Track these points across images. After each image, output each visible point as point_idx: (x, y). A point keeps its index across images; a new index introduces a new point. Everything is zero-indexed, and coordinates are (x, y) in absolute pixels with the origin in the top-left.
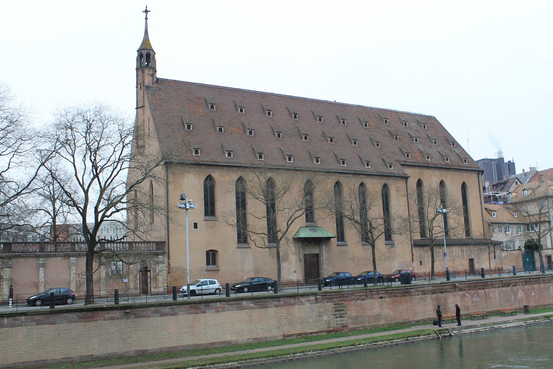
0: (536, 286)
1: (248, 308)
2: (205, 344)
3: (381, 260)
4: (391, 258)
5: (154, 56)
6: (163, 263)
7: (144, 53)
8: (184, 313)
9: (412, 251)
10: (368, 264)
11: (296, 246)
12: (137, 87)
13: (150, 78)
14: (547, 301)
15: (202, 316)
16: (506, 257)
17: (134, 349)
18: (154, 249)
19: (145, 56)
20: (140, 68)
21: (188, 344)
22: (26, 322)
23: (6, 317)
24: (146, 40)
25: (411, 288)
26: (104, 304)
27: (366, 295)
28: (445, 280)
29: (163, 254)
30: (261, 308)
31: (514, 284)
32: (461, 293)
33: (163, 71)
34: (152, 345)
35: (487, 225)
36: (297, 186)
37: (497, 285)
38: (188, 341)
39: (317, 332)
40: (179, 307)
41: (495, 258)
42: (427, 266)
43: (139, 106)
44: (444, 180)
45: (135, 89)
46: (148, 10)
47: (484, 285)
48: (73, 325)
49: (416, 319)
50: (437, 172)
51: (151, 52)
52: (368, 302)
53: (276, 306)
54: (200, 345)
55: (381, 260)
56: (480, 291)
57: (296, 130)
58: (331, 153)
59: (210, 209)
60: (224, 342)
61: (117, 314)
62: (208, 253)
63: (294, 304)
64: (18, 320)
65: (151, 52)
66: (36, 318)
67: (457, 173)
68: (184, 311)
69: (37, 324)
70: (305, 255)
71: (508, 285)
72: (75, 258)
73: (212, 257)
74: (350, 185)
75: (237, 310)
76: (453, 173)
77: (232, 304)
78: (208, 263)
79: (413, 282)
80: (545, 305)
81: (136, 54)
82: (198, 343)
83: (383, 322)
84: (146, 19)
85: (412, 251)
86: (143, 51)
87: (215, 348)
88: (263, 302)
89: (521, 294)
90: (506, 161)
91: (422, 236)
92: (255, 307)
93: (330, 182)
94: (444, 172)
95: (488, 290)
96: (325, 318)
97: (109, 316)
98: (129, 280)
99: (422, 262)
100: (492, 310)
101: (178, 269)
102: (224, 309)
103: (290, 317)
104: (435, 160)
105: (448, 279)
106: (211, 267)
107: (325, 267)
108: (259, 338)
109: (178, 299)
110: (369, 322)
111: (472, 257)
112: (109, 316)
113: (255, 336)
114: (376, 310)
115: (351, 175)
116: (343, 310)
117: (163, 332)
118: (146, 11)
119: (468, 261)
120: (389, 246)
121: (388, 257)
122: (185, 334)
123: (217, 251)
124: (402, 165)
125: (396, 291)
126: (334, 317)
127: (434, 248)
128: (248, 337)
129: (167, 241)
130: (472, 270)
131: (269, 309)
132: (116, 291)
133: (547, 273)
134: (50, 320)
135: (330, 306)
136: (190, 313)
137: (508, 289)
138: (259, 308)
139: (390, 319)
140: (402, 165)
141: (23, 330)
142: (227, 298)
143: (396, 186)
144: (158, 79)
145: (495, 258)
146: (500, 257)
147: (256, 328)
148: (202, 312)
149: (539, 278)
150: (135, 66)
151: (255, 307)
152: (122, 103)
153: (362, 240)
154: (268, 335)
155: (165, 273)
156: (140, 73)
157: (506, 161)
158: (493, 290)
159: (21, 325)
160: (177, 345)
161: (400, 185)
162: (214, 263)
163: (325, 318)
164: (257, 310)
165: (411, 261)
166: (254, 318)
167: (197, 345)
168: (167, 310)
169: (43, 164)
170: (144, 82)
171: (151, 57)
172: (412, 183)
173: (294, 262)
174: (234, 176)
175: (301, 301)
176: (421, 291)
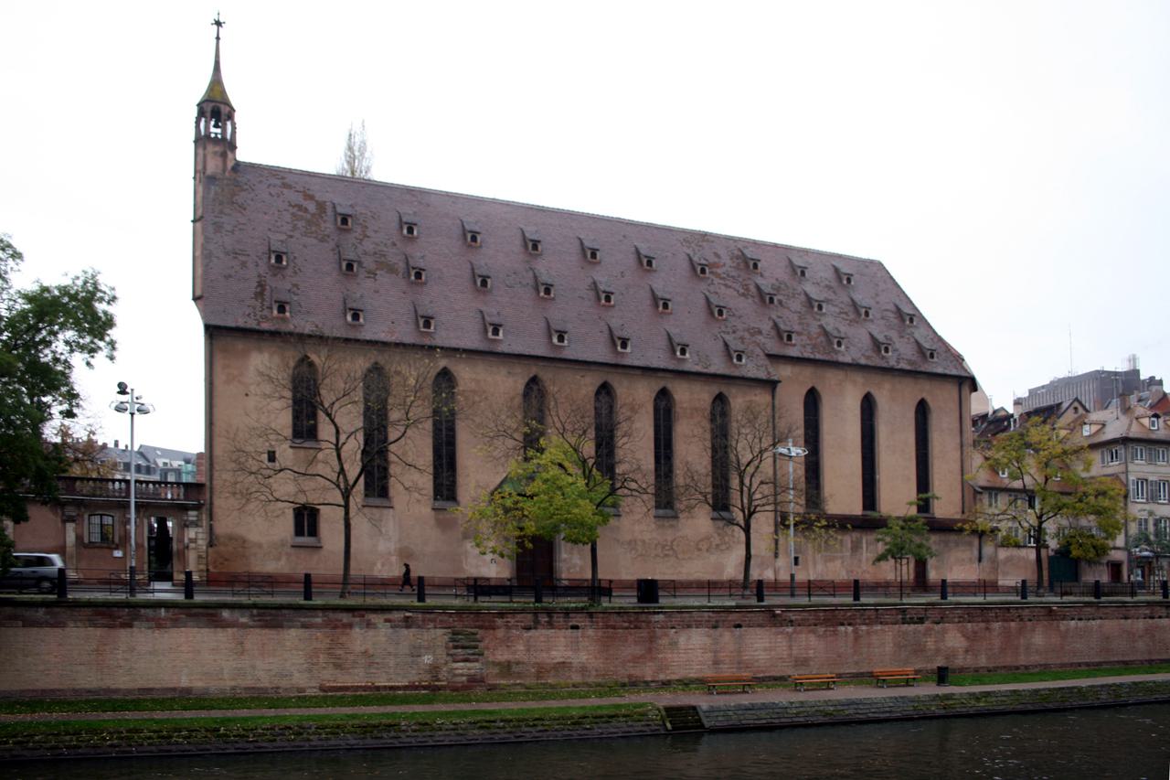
2: (129, 691)
3: (700, 550)
4: (723, 547)
6: (197, 526)
8: (79, 624)
10: (666, 555)
12: (195, 178)
13: (219, 161)
14: (1022, 657)
15: (123, 634)
16: (1008, 560)
18: (182, 497)
23: (165, 607)
24: (216, 81)
28: (850, 600)
29: (198, 507)
35: (972, 492)
36: (504, 385)
38: (88, 679)
39: (405, 688)
41: (980, 560)
45: (193, 181)
47: (942, 615)
50: (859, 378)
52: (540, 634)
54: (117, 691)
55: (700, 550)
57: (531, 274)
58: (603, 323)
60: (174, 689)
63: (350, 626)
65: (222, 107)
68: (80, 621)
74: (637, 397)
75: (207, 627)
78: (299, 531)
79: (949, 598)
80: (1017, 668)
82: (113, 687)
84: (218, 38)
87: (153, 700)
88: (271, 615)
90: (1144, 376)
91: (865, 507)
92: (251, 623)
93: (587, 385)
96: (427, 659)
98: (125, 554)
99: (800, 559)
101: (231, 538)
105: (856, 597)
107: (564, 556)
108: (259, 689)
110: (538, 678)
113: (249, 682)
115: (638, 372)
116: (476, 647)
117: (30, 659)
120: (721, 524)
121: (717, 545)
122: (82, 667)
126: (449, 658)
128: (233, 683)
129: (208, 484)
130: (921, 583)
131: (285, 631)
133: (1031, 599)
135: (439, 636)
136: (95, 626)
137: (920, 627)
140: (770, 356)
142: (187, 601)
144: (238, 164)
145: (980, 560)
146: (994, 560)
147: (253, 667)
149: (1008, 609)
151: (251, 623)
155: (202, 543)
156: (201, 151)
157: (1144, 376)
160: (61, 687)
162: (314, 532)
164: (258, 630)
165: (772, 554)
167: (108, 691)
170: (205, 168)
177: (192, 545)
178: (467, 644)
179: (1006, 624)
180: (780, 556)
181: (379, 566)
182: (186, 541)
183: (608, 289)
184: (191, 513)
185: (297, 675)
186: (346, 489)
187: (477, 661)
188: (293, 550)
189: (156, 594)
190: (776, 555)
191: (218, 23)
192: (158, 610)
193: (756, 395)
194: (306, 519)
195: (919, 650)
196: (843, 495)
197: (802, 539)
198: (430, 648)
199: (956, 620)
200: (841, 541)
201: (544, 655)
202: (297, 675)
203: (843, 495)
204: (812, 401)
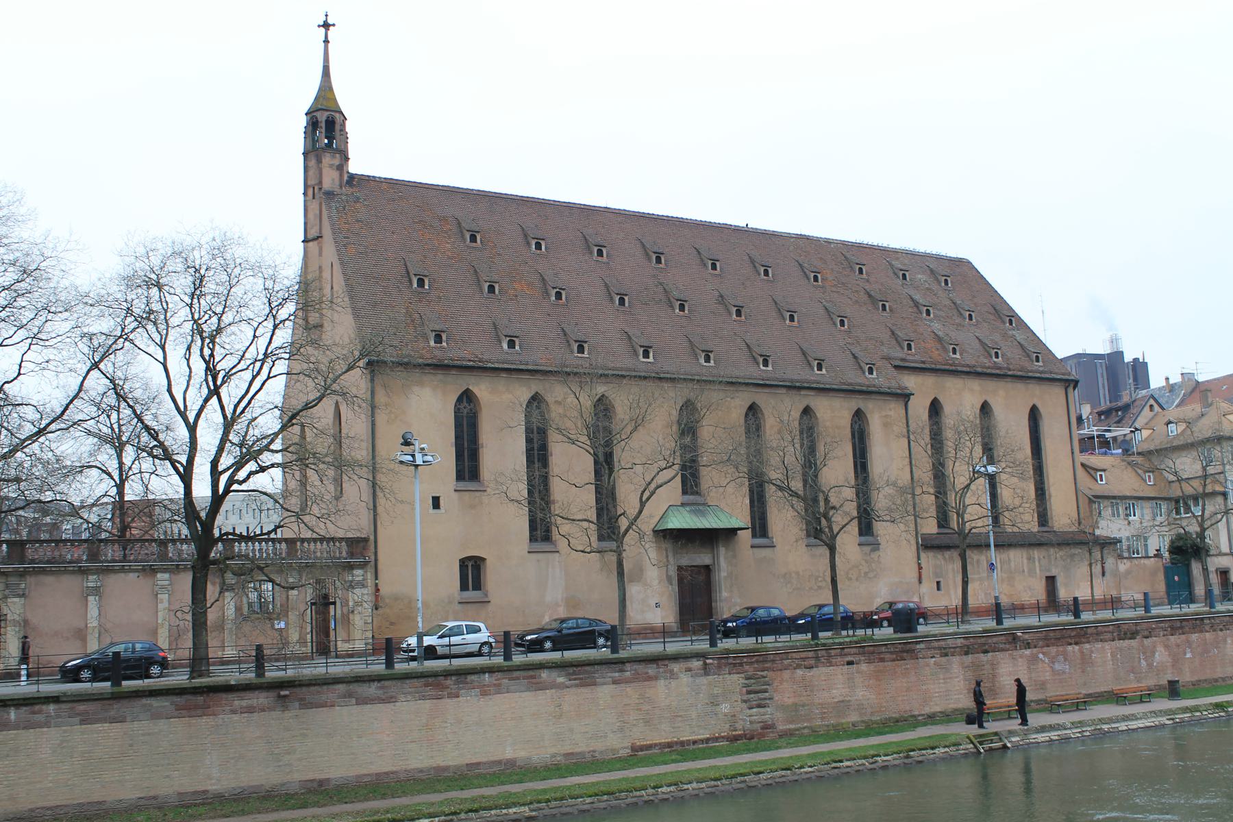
0: (1194, 637)
1: (554, 686)
2: (458, 767)
3: (850, 579)
4: (871, 575)
5: (343, 125)
6: (364, 586)
7: (322, 117)
8: (409, 697)
10: (820, 588)
11: (659, 549)
12: (305, 194)
13: (336, 174)
15: (449, 703)
16: (1128, 572)
17: (298, 777)
18: (344, 554)
19: (323, 125)
20: (312, 152)
21: (420, 766)
22: (58, 716)
23: (14, 705)
24: (326, 88)
25: (917, 643)
26: (233, 676)
27: (817, 658)
28: (992, 624)
29: (363, 566)
30: (582, 685)
31: (1146, 633)
32: (1028, 652)
33: (364, 158)
34: (338, 769)
36: (662, 414)
37: (1109, 636)
38: (419, 759)
39: (707, 740)
40: (399, 683)
41: (1103, 574)
42: (952, 592)
43: (310, 237)
45: (302, 198)
46: (330, 22)
47: (1080, 634)
48: (162, 724)
49: (927, 710)
50: (975, 384)
51: (337, 115)
52: (821, 672)
53: (615, 682)
54: (446, 769)
55: (850, 579)
56: (1070, 648)
57: (660, 289)
58: (739, 340)
59: (468, 465)
60: (500, 762)
61: (261, 699)
62: (463, 563)
63: (656, 678)
64: (40, 712)
65: (337, 115)
66: (81, 707)
67: (1020, 386)
68: (410, 693)
69: (82, 722)
70: (680, 568)
71: (1133, 635)
72: (167, 576)
73: (472, 572)
75: (528, 690)
77: (518, 678)
78: (464, 587)
79: (920, 628)
80: (1216, 680)
81: (303, 121)
82: (442, 764)
83: (854, 717)
84: (326, 41)
85: (919, 558)
86: (318, 114)
89: (1161, 655)
90: (1128, 358)
92: (568, 683)
93: (737, 404)
94: (991, 384)
95: (1087, 646)
96: (725, 708)
97: (244, 703)
98: (287, 624)
99: (942, 584)
100: (1098, 690)
101: (396, 598)
102: (499, 689)
103: (646, 707)
104: (970, 356)
106: (471, 595)
107: (725, 594)
108: (577, 754)
109: (397, 666)
110: (823, 718)
111: (1053, 572)
112: (244, 703)
114: (838, 691)
115: (784, 391)
116: (766, 691)
118: (326, 26)
119: (1044, 580)
121: (866, 573)
123: (483, 560)
124: (896, 367)
125: (883, 649)
126: (745, 706)
127: (968, 553)
128: (554, 750)
129: (372, 538)
130: (1052, 603)
131: (599, 689)
132: (259, 648)
133: (1220, 607)
134: (112, 713)
135: (735, 681)
136: (423, 698)
137: (1133, 643)
138: (577, 686)
139: (869, 710)
140: (896, 367)
141: (51, 735)
143: (884, 413)
144: (352, 177)
145: (1103, 574)
146: (1116, 573)
147: (571, 730)
148: (451, 696)
149: (1202, 619)
150: (300, 148)
151: (568, 683)
152: (271, 229)
153: (808, 535)
154: (599, 746)
155: (367, 608)
156: (312, 163)
157: (1128, 358)
158: (1099, 645)
159: (47, 724)
160: (394, 769)
161: (892, 413)
162: (478, 586)
163: (725, 708)
164: (573, 690)
165: (916, 580)
166: (566, 707)
168: (372, 690)
169: (96, 365)
170: (320, 183)
171: (337, 127)
172: (919, 407)
173: (656, 582)
174: (522, 392)
175: (671, 671)
176: (940, 648)
178: (758, 688)
179: (1202, 635)
180: (924, 581)
183: (682, 297)
184: (159, 575)
188: (459, 607)
192: (482, 676)
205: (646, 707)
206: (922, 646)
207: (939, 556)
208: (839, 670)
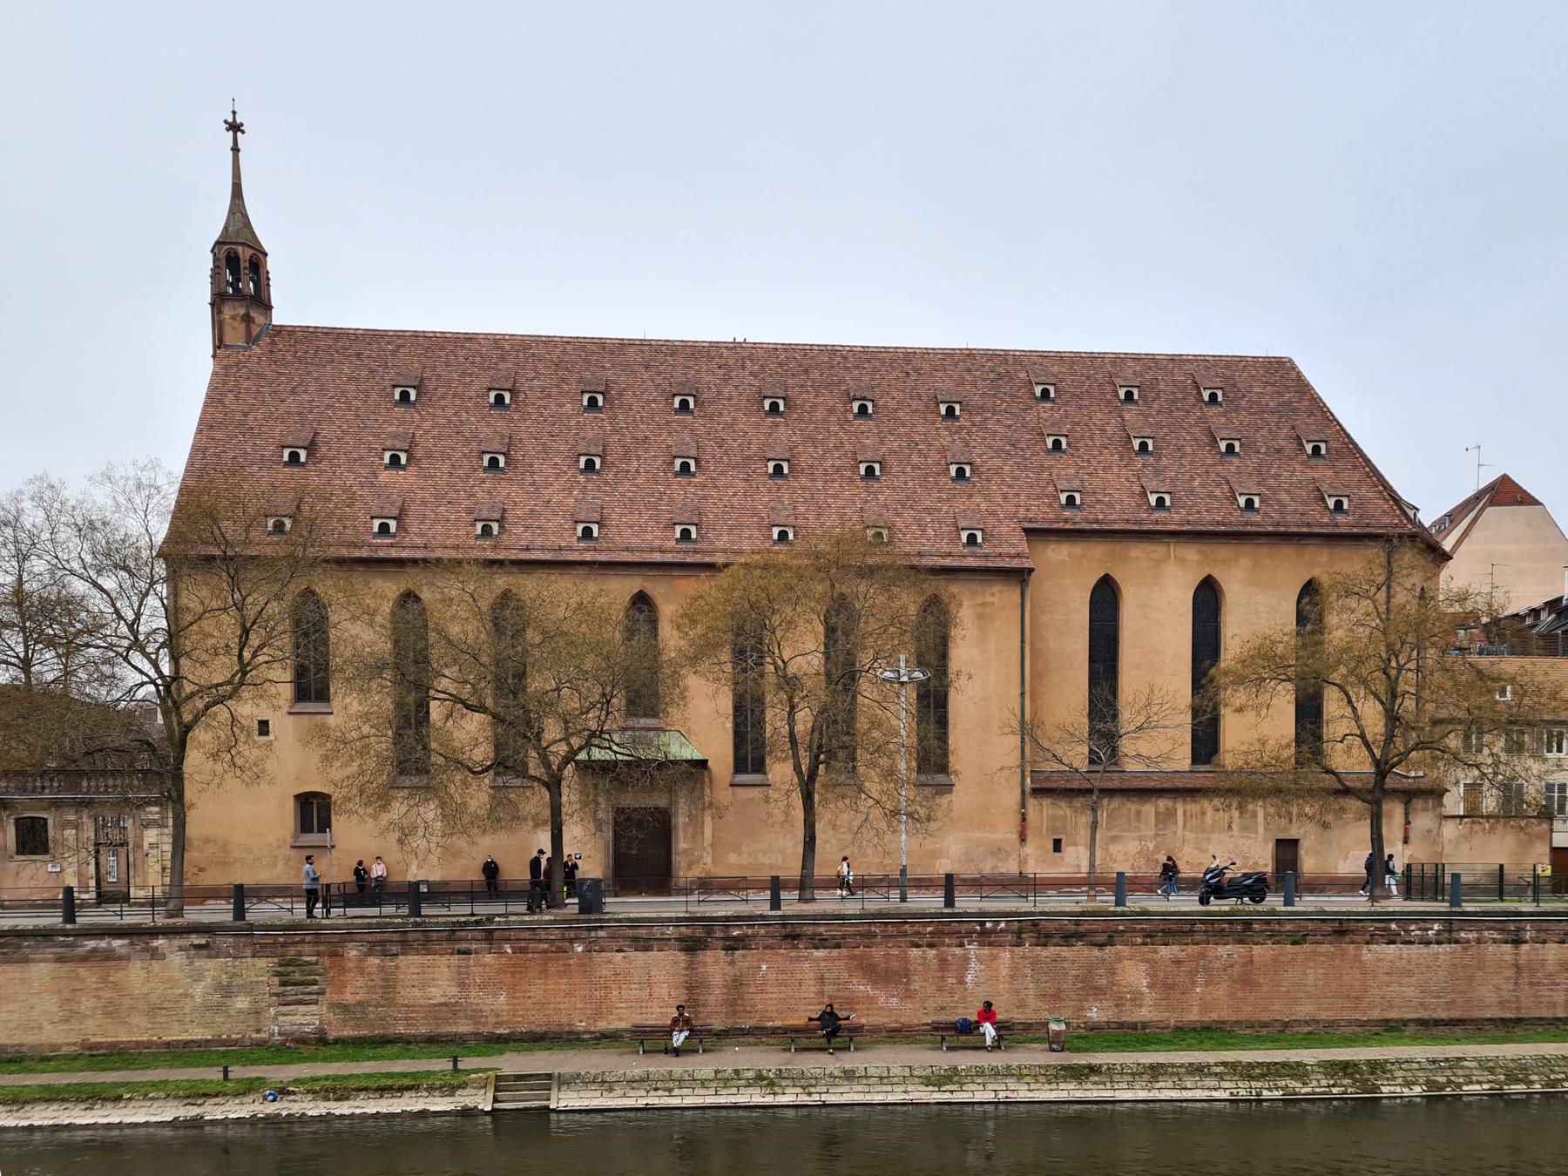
6: (161, 826)
9: (1023, 805)
25: (595, 929)
27: (404, 942)
31: (1101, 939)
33: (289, 307)
44: (1216, 575)
49: (602, 1025)
50: (1191, 552)
53: (60, 960)
56: (914, 952)
67: (1288, 551)
70: (619, 811)
72: (156, 809)
76: (1264, 550)
84: (236, 149)
85: (1023, 805)
91: (1196, 759)
94: (1223, 551)
103: (108, 994)
111: (1293, 833)
116: (315, 983)
119: (1271, 846)
135: (259, 969)
139: (492, 1019)
143: (979, 600)
149: (1248, 923)
154: (30, 1039)
161: (994, 600)
163: (242, 1003)
165: (1015, 837)
176: (635, 939)
177: (154, 852)
180: (1029, 838)
181: (414, 868)
182: (146, 845)
185: (47, 1027)
186: (552, 776)
187: (316, 1002)
189: (912, 895)
190: (1023, 839)
191: (235, 127)
193: (993, 595)
194: (313, 811)
195: (1246, 980)
196: (1158, 742)
197: (1068, 812)
198: (249, 989)
199: (1139, 940)
200: (1139, 812)
201: (417, 992)
202: (47, 1027)
203: (1158, 742)
204: (1105, 598)
205: (108, 994)
206: (602, 934)
207: (1063, 804)
208: (444, 961)
